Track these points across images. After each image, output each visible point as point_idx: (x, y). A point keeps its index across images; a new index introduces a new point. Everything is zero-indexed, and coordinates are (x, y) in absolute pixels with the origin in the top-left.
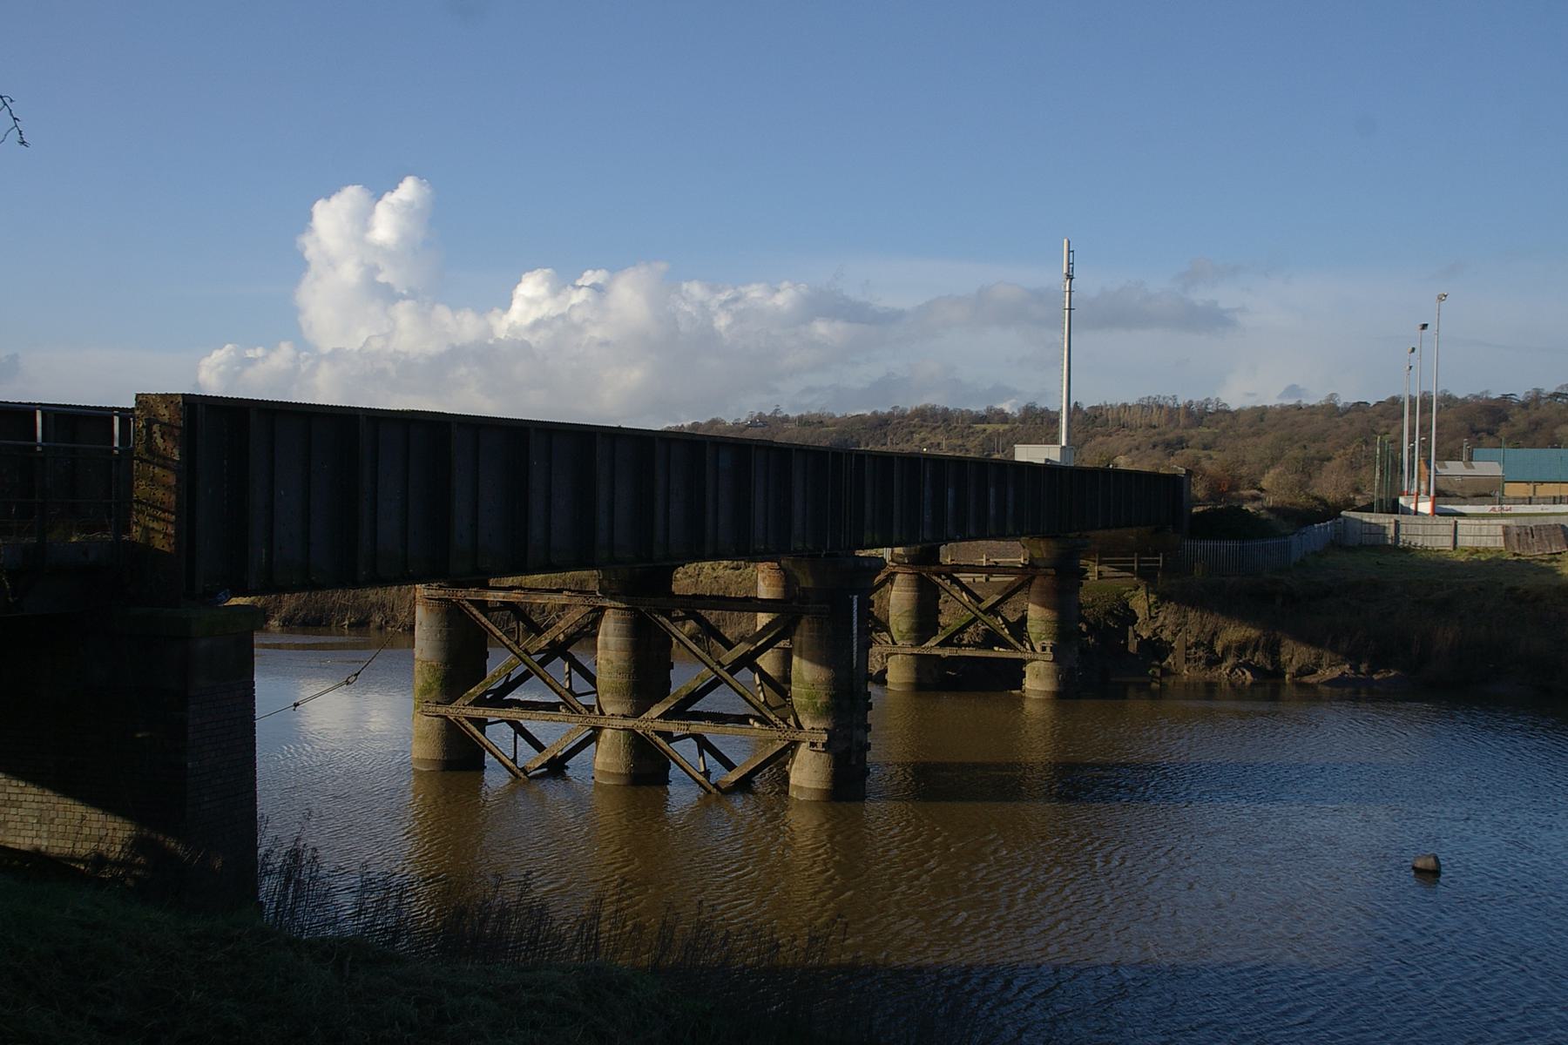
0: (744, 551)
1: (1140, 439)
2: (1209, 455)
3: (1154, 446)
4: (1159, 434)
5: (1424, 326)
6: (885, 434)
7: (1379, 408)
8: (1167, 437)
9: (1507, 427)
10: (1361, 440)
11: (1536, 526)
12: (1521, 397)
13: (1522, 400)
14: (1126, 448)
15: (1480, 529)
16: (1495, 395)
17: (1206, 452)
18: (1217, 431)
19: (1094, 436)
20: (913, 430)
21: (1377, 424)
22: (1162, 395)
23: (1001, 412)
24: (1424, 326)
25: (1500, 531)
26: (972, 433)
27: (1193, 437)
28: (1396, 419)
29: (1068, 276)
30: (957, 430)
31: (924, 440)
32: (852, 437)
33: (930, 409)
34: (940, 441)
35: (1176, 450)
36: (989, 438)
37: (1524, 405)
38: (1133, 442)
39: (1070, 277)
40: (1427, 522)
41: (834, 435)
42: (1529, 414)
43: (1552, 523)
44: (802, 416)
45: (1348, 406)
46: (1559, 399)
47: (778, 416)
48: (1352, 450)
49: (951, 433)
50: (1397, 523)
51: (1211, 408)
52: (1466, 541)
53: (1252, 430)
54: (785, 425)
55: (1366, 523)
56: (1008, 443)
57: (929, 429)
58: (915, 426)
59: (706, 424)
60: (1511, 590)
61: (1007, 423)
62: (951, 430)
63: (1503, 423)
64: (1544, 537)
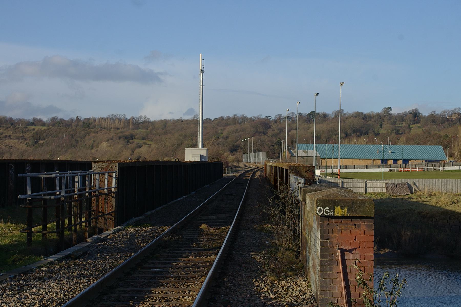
0: (20, 199)
2: (145, 142)
3: (120, 138)
4: (121, 132)
5: (317, 94)
9: (271, 131)
10: (216, 136)
11: (398, 183)
13: (273, 119)
15: (376, 185)
16: (263, 117)
18: (147, 131)
19: (89, 133)
21: (217, 129)
22: (119, 114)
23: (40, 121)
24: (317, 94)
25: (384, 185)
26: (28, 130)
27: (137, 134)
28: (224, 127)
29: (202, 71)
30: (20, 129)
34: (11, 134)
35: (130, 140)
36: (37, 133)
37: (275, 122)
38: (109, 136)
39: (203, 71)
40: (354, 182)
42: (278, 126)
43: (404, 182)
48: (212, 141)
49: (16, 130)
50: (342, 182)
51: (142, 120)
52: (370, 190)
55: (330, 182)
56: (46, 136)
57: (5, 128)
60: (420, 213)
62: (16, 129)
63: (269, 129)
64: (401, 188)
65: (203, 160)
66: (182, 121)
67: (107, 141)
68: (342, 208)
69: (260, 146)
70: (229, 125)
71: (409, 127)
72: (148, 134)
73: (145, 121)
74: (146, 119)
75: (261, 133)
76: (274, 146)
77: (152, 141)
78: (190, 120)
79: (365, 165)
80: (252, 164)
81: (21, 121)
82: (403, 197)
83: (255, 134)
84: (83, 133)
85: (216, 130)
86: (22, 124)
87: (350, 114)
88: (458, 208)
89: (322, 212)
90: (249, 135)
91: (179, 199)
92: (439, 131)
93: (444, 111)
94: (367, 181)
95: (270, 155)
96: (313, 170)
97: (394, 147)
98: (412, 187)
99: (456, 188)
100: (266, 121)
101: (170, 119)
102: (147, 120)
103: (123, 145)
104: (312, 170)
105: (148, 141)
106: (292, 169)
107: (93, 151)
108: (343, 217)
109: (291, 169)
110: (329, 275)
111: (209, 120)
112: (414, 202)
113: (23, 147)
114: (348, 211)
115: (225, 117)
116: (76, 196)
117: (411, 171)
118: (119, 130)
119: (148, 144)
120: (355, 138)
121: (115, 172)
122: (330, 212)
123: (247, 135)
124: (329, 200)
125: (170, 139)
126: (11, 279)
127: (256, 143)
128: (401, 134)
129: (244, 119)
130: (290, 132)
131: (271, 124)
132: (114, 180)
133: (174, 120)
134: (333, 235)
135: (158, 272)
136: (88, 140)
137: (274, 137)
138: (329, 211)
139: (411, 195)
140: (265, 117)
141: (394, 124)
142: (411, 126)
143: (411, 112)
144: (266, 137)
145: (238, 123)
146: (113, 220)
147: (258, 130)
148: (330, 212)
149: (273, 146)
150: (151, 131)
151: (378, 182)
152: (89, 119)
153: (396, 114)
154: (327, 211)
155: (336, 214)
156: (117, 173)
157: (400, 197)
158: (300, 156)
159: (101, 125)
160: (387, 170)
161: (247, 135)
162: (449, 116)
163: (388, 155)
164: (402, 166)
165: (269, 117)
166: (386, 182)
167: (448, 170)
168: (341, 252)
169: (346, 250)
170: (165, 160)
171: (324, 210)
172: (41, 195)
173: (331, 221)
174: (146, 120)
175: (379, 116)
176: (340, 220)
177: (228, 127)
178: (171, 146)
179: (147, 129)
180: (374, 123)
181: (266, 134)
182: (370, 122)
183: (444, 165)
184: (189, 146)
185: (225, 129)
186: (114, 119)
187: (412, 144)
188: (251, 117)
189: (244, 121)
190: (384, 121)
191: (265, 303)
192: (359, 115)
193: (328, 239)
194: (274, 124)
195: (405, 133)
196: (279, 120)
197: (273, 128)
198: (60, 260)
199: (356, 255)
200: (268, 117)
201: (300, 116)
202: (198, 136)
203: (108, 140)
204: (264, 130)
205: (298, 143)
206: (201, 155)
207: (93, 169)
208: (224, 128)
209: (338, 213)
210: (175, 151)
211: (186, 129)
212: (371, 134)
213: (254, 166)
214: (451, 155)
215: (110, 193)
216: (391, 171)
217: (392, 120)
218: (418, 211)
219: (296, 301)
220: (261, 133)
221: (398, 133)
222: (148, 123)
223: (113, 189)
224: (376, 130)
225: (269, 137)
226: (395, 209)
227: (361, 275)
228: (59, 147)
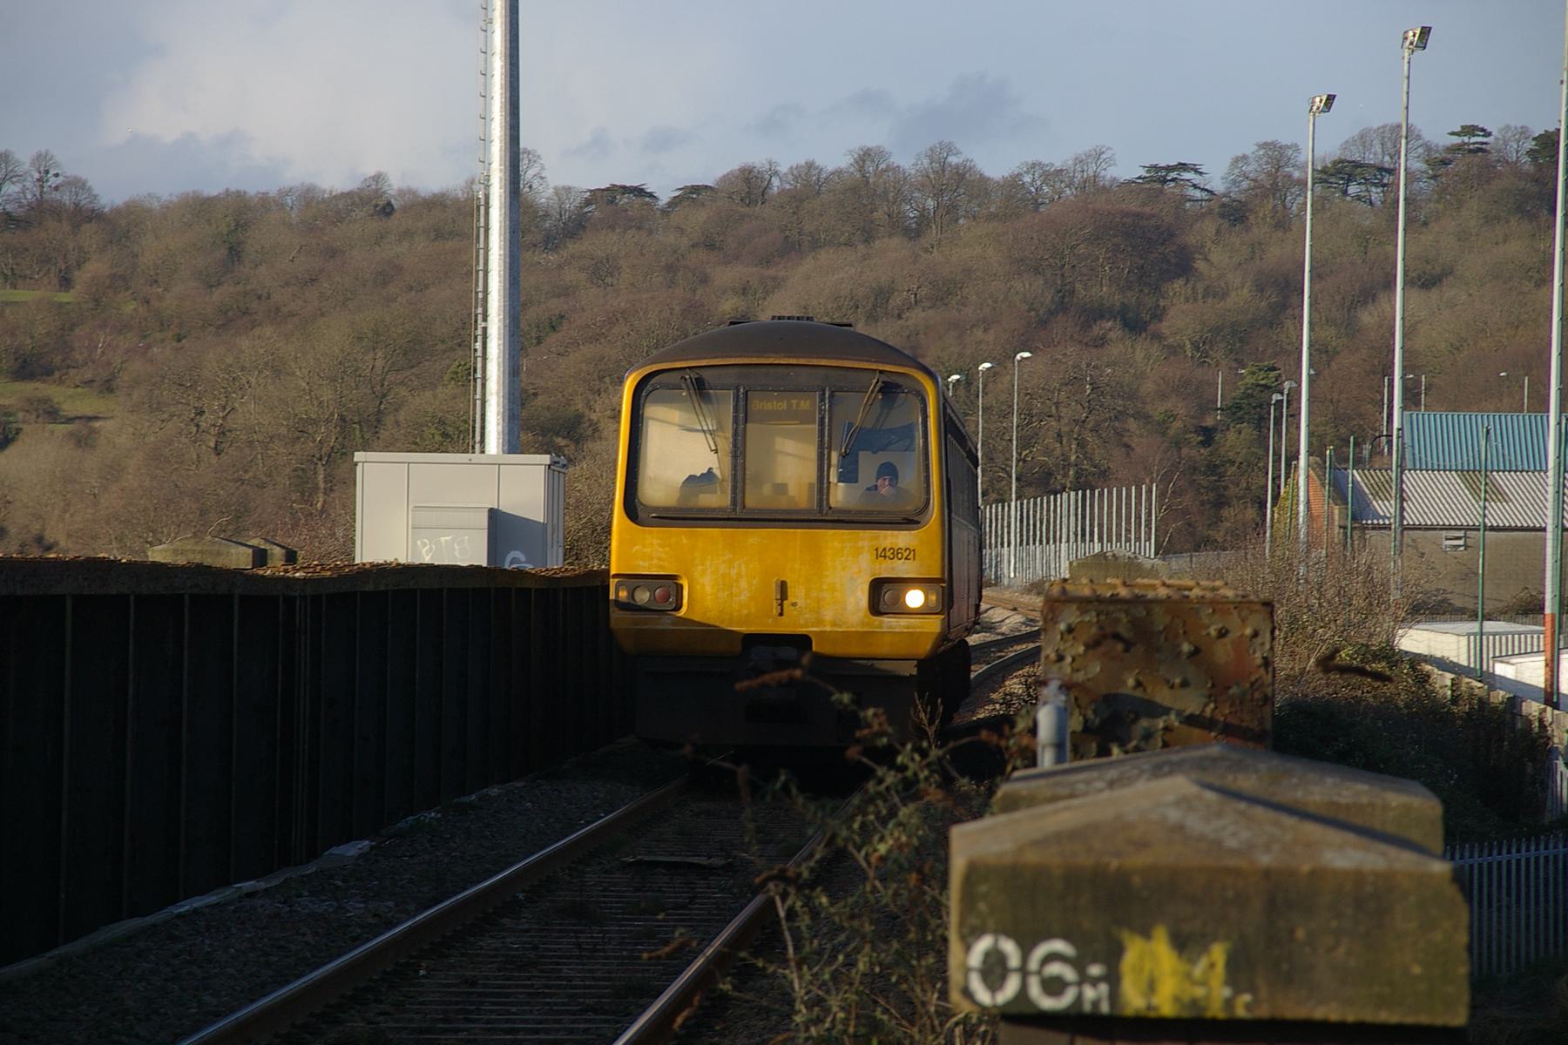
2: (47, 400)
7: (699, 218)
12: (1217, 176)
13: (1218, 186)
16: (1126, 167)
17: (29, 388)
18: (65, 297)
21: (705, 280)
28: (767, 261)
37: (1234, 212)
45: (571, 204)
46: (1353, 189)
53: (217, 296)
63: (1178, 284)
65: (516, 560)
66: (387, 210)
68: (1183, 944)
69: (1089, 437)
70: (816, 245)
72: (73, 326)
73: (40, 201)
74: (53, 181)
76: (1218, 436)
77: (108, 387)
78: (457, 200)
80: (1007, 595)
83: (1043, 323)
85: (694, 291)
89: (1011, 987)
90: (991, 336)
91: (185, 907)
95: (1185, 512)
96: (1256, 634)
100: (1147, 210)
101: (273, 192)
102: (66, 198)
104: (1248, 631)
105: (71, 391)
106: (1070, 630)
109: (1062, 626)
111: (638, 200)
114: (1238, 972)
115: (776, 173)
119: (70, 420)
122: (1080, 984)
123: (979, 333)
125: (277, 370)
127: (1057, 404)
130: (1370, 306)
131: (1191, 240)
133: (308, 197)
138: (1069, 973)
140: (1143, 173)
144: (1147, 357)
145: (897, 225)
147: (1078, 286)
148: (1084, 979)
149: (1208, 436)
150: (97, 301)
154: (1055, 969)
155: (1134, 1000)
158: (1428, 528)
161: (979, 333)
165: (1183, 167)
170: (158, 554)
171: (1033, 964)
174: (57, 195)
177: (808, 264)
178: (283, 431)
179: (66, 282)
181: (1152, 327)
184: (445, 435)
185: (774, 279)
188: (1019, 174)
189: (952, 209)
194: (1218, 232)
197: (1214, 274)
200: (1169, 169)
201: (1470, 158)
202: (479, 345)
204: (1129, 294)
205: (1404, 408)
206: (494, 515)
208: (772, 272)
209: (1152, 987)
210: (322, 485)
211: (427, 287)
213: (1017, 619)
220: (1102, 317)
222: (76, 227)
225: (1174, 350)
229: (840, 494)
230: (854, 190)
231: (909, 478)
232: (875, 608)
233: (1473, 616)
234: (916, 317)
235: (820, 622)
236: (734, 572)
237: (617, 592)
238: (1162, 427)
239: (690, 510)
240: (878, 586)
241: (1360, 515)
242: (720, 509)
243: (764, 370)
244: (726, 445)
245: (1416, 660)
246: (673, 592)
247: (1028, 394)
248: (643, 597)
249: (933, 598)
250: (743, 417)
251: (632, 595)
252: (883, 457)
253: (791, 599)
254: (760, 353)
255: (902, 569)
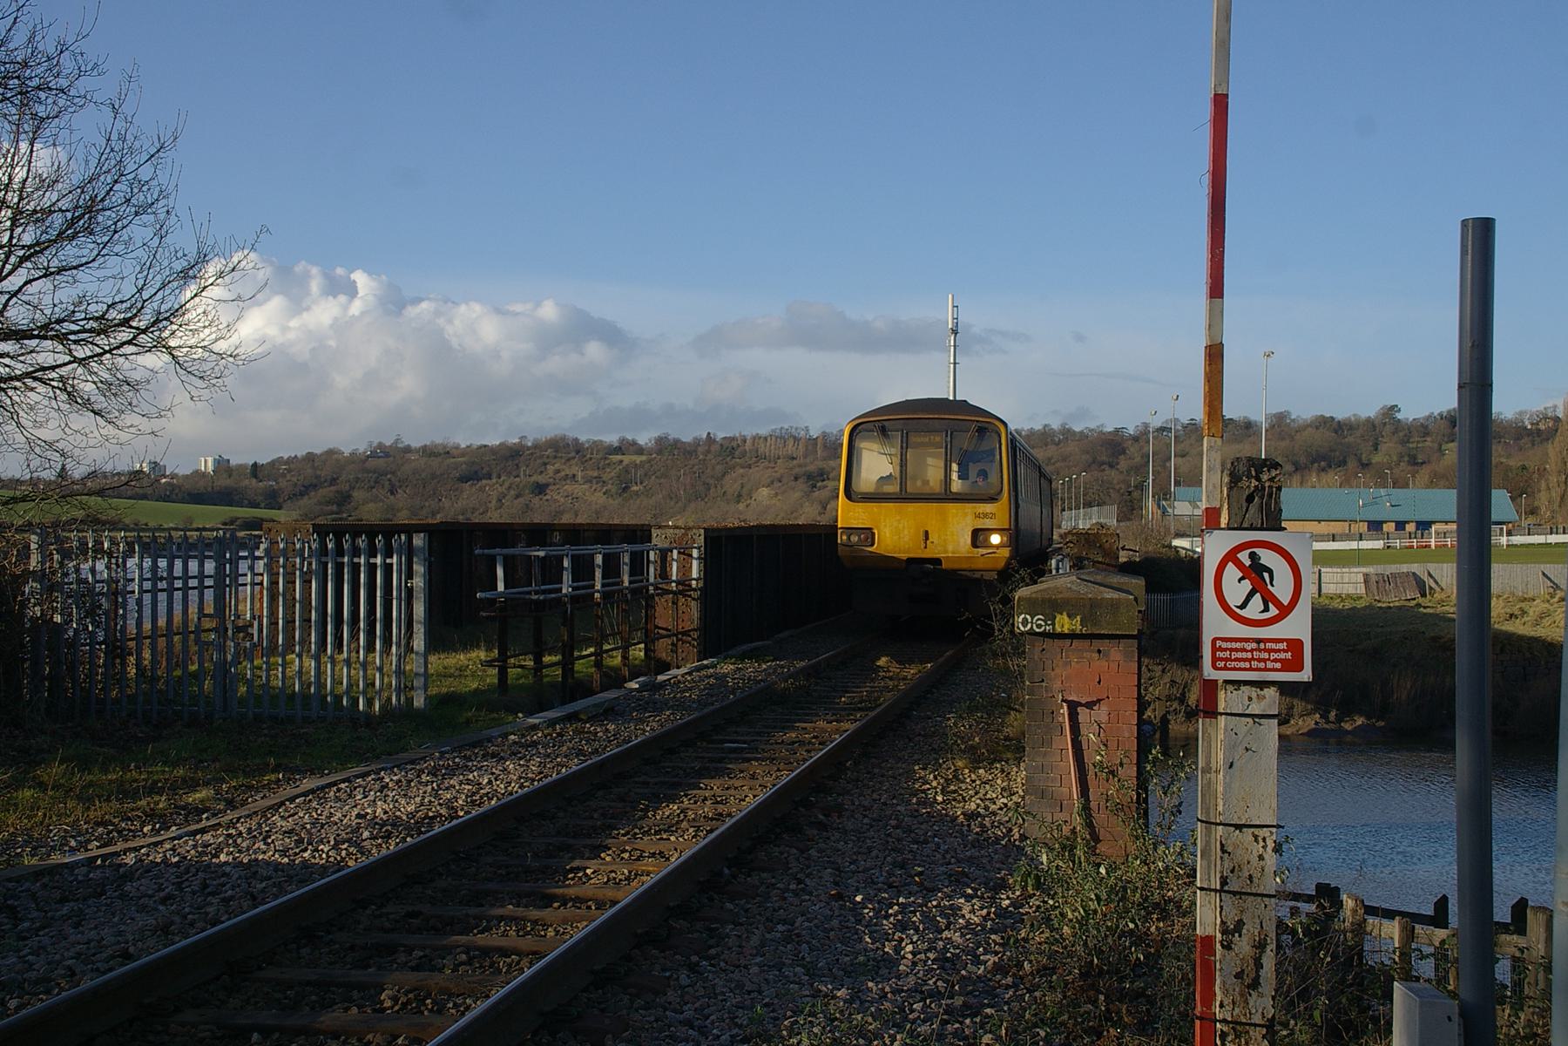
0: (481, 599)
1: (782, 471)
3: (796, 479)
4: (800, 466)
6: (517, 465)
8: (808, 468)
14: (769, 480)
15: (1342, 577)
16: (1109, 429)
20: (547, 461)
23: (634, 443)
25: (1361, 578)
26: (609, 464)
31: (558, 471)
32: (482, 468)
33: (561, 439)
34: (575, 473)
37: (1135, 439)
41: (464, 466)
43: (1405, 571)
44: (426, 446)
47: (400, 445)
54: (408, 456)
56: (646, 475)
57: (563, 461)
58: (548, 457)
59: (321, 455)
60: (1435, 639)
61: (642, 454)
67: (769, 486)
71: (1440, 449)
75: (1103, 463)
79: (1328, 535)
81: (597, 445)
82: (1402, 603)
84: (719, 468)
86: (598, 451)
87: (1305, 420)
88: (1522, 627)
92: (1509, 456)
93: (1521, 413)
94: (1323, 570)
97: (1398, 494)
98: (1424, 582)
99: (1524, 585)
103: (802, 494)
107: (741, 506)
108: (1072, 636)
110: (1045, 754)
112: (1425, 614)
113: (599, 498)
116: (597, 595)
117: (1433, 547)
118: (795, 462)
120: (1314, 474)
121: (699, 548)
124: (1043, 601)
126: (442, 754)
128: (1422, 463)
129: (1067, 433)
132: (695, 563)
134: (1053, 674)
135: (734, 750)
136: (731, 484)
137: (1132, 473)
138: (1043, 623)
139: (1421, 600)
141: (1404, 442)
142: (1443, 447)
143: (1445, 414)
146: (693, 646)
148: (1046, 624)
149: (1130, 493)
151: (1347, 570)
152: (733, 439)
153: (1411, 419)
154: (1039, 622)
156: (702, 549)
157: (1397, 604)
159: (757, 451)
160: (1379, 544)
162: (1532, 424)
163: (1384, 511)
164: (1413, 536)
166: (1364, 570)
167: (1519, 543)
168: (1068, 708)
169: (1081, 704)
172: (529, 593)
173: (1048, 643)
175: (1370, 424)
176: (1068, 642)
180: (1359, 441)
182: (1350, 439)
183: (1509, 534)
186: (783, 438)
187: (1445, 487)
190: (1383, 436)
191: (917, 811)
192: (1324, 422)
193: (1043, 681)
195: (1429, 462)
196: (1140, 437)
198: (552, 723)
199: (1101, 713)
203: (772, 483)
207: (654, 541)
209: (1063, 626)
212: (1352, 464)
214: (1533, 511)
215: (688, 591)
216: (1388, 547)
217: (1401, 434)
218: (1432, 634)
219: (986, 808)
221: (1413, 462)
223: (694, 582)
224: (1364, 456)
225: (1122, 472)
226: (1380, 630)
227: (1103, 753)
228: (671, 498)
229: (957, 485)
230: (1042, 434)
231: (993, 478)
232: (975, 544)
233: (1189, 536)
234: (1058, 465)
235: (946, 552)
236: (901, 526)
237: (842, 538)
238: (1118, 491)
239: (878, 494)
240: (976, 533)
241: (1164, 512)
242: (893, 494)
243: (915, 421)
244: (897, 460)
245: (1176, 547)
246: (870, 536)
247: (1085, 483)
248: (855, 539)
249: (1005, 539)
250: (905, 447)
251: (849, 539)
252: (980, 466)
253: (931, 539)
254: (914, 413)
255: (988, 524)
